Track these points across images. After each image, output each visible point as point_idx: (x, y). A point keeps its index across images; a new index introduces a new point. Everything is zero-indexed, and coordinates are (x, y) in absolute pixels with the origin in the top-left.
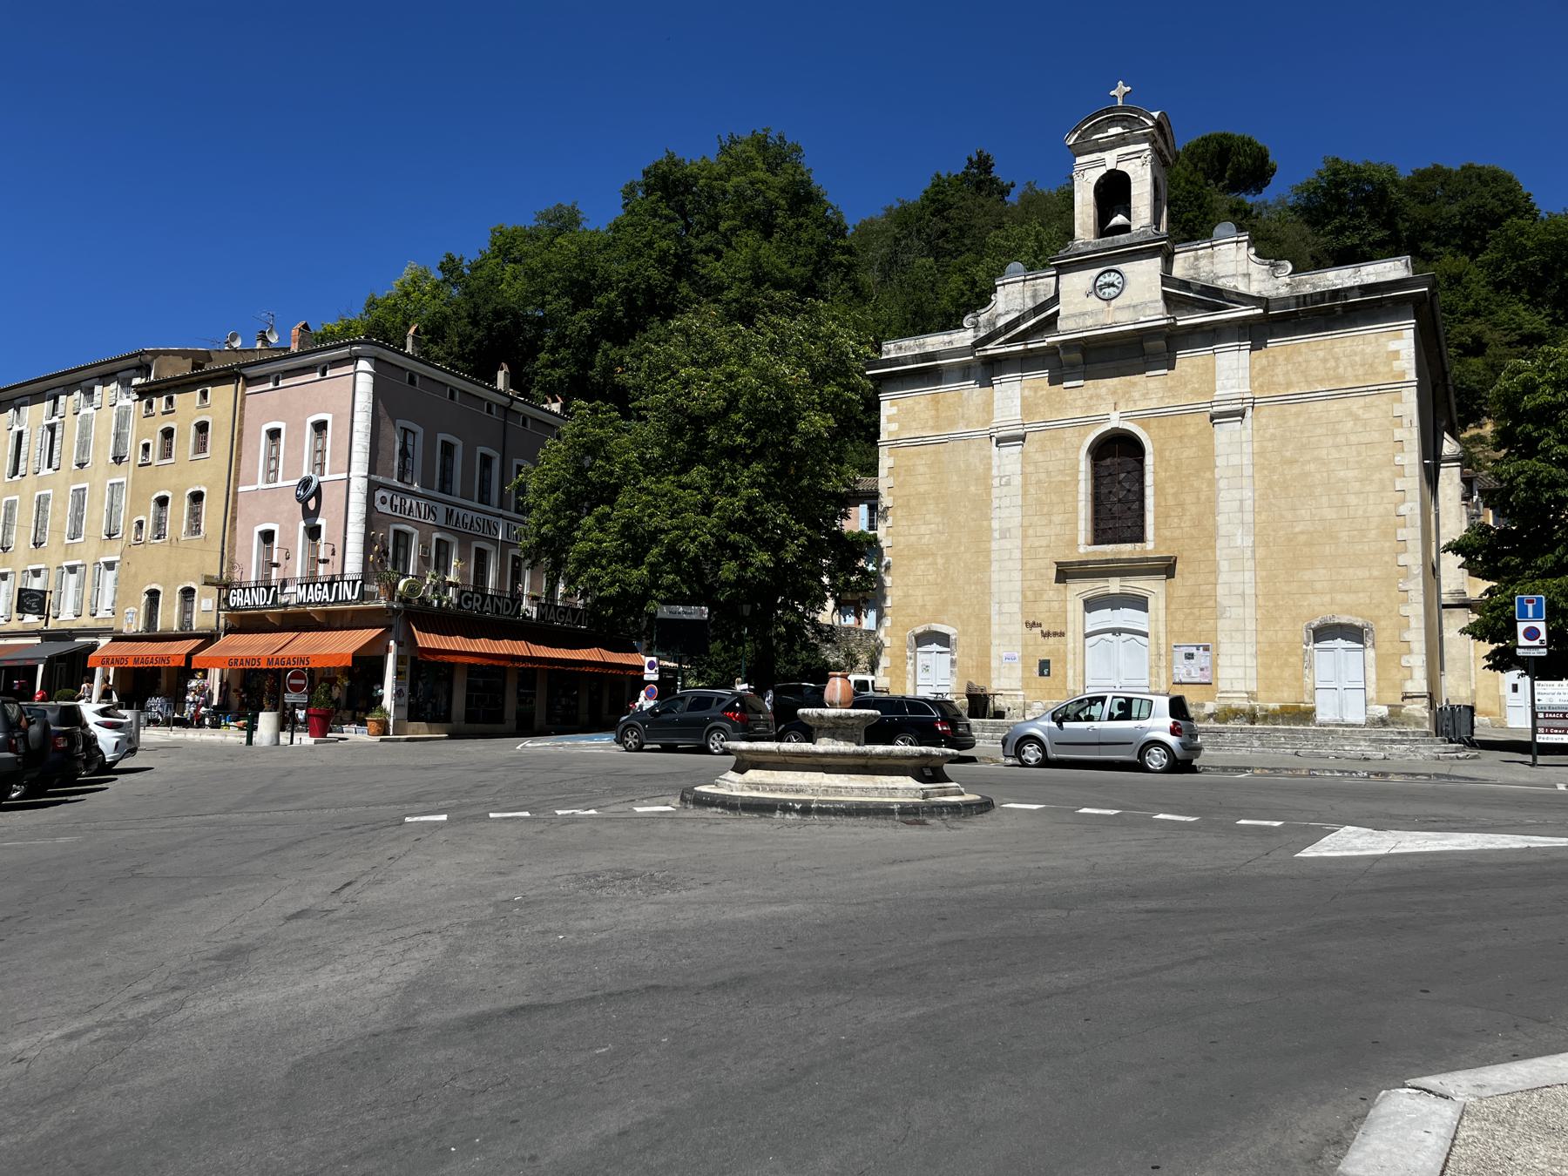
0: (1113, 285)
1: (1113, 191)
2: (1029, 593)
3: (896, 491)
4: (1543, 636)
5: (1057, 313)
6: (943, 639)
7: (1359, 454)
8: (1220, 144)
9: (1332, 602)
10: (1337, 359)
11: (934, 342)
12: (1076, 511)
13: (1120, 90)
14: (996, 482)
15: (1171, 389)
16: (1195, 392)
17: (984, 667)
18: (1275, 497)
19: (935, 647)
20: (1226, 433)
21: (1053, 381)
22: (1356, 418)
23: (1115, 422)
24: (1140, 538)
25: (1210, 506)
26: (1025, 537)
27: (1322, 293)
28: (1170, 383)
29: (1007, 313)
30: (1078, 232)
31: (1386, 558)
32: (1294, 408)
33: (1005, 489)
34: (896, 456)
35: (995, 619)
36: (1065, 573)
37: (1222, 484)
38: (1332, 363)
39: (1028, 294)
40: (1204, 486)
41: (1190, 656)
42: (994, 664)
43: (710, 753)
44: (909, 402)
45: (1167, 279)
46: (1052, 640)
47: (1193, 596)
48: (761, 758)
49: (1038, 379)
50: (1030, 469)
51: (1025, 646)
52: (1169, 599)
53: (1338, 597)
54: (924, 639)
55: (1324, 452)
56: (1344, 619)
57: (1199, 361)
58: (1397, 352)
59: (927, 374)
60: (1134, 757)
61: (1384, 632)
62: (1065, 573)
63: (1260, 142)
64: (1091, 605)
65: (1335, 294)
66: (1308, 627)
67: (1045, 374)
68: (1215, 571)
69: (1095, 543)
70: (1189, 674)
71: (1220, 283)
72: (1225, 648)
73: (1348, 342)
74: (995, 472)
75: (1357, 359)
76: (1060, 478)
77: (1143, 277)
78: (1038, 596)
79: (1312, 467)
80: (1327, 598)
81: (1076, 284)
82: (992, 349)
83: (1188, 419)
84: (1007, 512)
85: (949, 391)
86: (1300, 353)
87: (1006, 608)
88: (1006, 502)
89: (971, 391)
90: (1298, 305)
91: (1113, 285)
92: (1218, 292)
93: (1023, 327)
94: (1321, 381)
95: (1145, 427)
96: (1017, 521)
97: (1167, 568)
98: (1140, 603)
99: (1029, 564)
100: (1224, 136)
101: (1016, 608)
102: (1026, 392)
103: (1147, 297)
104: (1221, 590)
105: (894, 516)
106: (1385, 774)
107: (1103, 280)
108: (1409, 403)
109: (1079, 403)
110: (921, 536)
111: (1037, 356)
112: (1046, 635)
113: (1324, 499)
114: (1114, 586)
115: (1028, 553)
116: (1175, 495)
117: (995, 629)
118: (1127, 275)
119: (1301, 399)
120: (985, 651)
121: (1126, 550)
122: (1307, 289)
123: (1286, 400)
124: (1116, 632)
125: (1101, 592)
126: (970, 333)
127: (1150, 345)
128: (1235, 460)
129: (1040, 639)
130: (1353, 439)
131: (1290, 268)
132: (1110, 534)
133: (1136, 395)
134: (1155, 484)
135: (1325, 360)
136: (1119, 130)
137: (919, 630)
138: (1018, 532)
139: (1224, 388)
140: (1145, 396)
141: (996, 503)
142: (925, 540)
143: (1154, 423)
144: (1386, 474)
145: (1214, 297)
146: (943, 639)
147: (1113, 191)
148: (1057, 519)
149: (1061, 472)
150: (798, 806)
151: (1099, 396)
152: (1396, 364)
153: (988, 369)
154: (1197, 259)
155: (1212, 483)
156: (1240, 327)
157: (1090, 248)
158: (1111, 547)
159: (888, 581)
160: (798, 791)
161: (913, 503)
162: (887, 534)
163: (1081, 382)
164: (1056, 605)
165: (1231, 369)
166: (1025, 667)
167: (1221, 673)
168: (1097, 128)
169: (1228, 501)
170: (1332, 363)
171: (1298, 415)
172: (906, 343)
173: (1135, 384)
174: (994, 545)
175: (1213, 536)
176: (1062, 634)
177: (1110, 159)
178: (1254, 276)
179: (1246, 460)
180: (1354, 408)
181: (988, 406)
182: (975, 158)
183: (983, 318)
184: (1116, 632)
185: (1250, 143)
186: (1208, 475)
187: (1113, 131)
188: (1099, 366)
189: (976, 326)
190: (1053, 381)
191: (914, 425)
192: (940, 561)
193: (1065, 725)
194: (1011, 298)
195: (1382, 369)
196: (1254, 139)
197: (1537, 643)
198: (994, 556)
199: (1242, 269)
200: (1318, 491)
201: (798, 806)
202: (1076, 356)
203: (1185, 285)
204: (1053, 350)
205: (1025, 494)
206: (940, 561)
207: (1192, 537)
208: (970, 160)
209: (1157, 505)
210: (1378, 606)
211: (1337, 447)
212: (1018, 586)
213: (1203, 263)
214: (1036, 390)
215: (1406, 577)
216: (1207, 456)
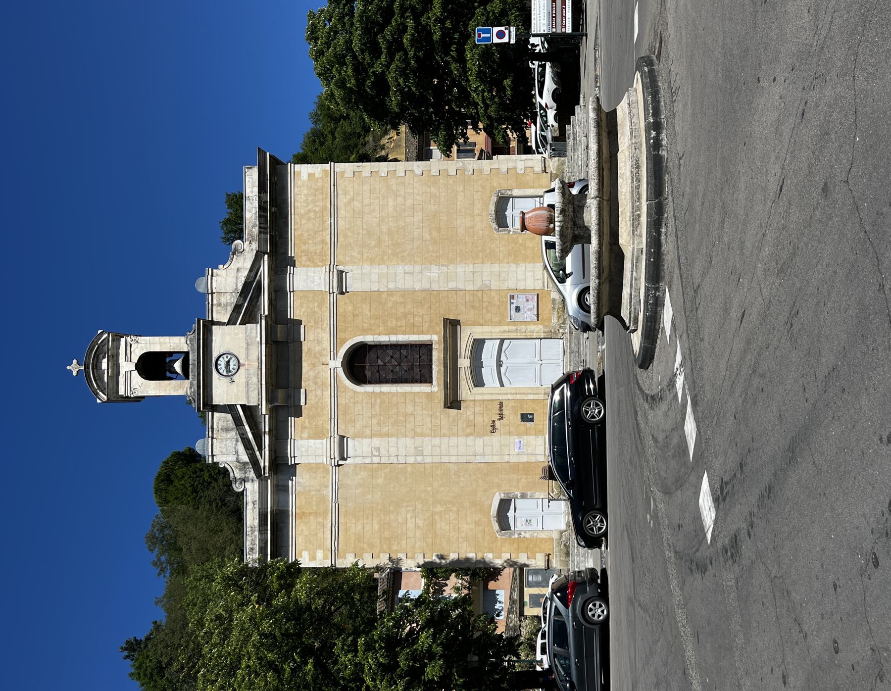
0: (228, 362)
1: (154, 366)
2: (468, 431)
3: (376, 551)
4: (503, 28)
5: (242, 406)
6: (505, 505)
7: (378, 198)
8: (163, 481)
9: (480, 215)
10: (309, 211)
11: (251, 518)
12: (404, 394)
13: (74, 368)
14: (376, 460)
15: (316, 323)
16: (320, 306)
17: (526, 468)
18: (404, 252)
19: (511, 514)
20: (353, 284)
21: (298, 413)
22: (353, 199)
23: (337, 363)
24: (427, 347)
25: (408, 294)
26: (422, 435)
27: (260, 216)
28: (312, 323)
29: (237, 452)
30: (181, 392)
31: (451, 182)
32: (341, 239)
33: (383, 452)
34: (345, 552)
35: (488, 459)
36: (453, 402)
37: (391, 286)
38: (312, 215)
39: (224, 434)
40: (393, 299)
41: (518, 309)
42: (524, 459)
43: (607, 618)
44: (300, 540)
45: (232, 322)
46: (505, 412)
47: (473, 307)
48: (606, 230)
49: (294, 423)
50: (368, 431)
51: (510, 433)
52: (475, 323)
53: (477, 212)
54: (504, 523)
55: (374, 219)
56: (492, 208)
57: (297, 303)
58: (309, 175)
59: (278, 524)
60: (597, 629)
61: (502, 185)
62: (453, 402)
63: (167, 456)
64: (478, 382)
65: (262, 208)
66: (497, 231)
67: (292, 420)
68: (456, 291)
69: (431, 382)
70: (531, 310)
71: (240, 287)
72: (512, 285)
73: (298, 204)
74: (367, 461)
75: (310, 199)
76: (377, 407)
77: (224, 339)
78: (470, 424)
79: (384, 228)
80: (478, 219)
81: (223, 391)
82: (265, 462)
83: (340, 310)
84: (400, 449)
85: (295, 503)
86: (302, 235)
87: (479, 450)
88: (393, 451)
89: (299, 484)
90: (266, 233)
91: (228, 362)
92: (247, 285)
93: (250, 436)
94: (324, 222)
95: (344, 341)
96: (409, 441)
97: (452, 326)
98: (478, 345)
99: (445, 431)
100: (157, 479)
101: (480, 442)
102: (305, 435)
103: (242, 336)
104: (470, 287)
105: (397, 552)
106: (596, 77)
107: (223, 370)
108: (346, 169)
109: (319, 393)
110: (417, 526)
111: (277, 428)
112: (501, 417)
113: (408, 220)
114: (464, 363)
115: (436, 432)
116: (398, 319)
117: (496, 459)
118: (222, 352)
119: (334, 234)
120: (515, 468)
121: (437, 356)
122: (256, 231)
123: (334, 245)
124: (499, 364)
125: (469, 374)
126: (248, 485)
127: (280, 336)
128: (374, 277)
129: (505, 421)
130: (366, 201)
131: (239, 241)
132: (425, 371)
133: (318, 348)
134: (388, 334)
135: (309, 219)
136: (105, 361)
137: (496, 527)
138: (418, 441)
139: (320, 284)
140: (319, 342)
141: (393, 460)
142: (420, 522)
143: (341, 335)
144: (393, 182)
145: (250, 289)
146: (505, 505)
147: (154, 366)
148: (410, 409)
149: (373, 406)
150: (653, 134)
151: (316, 377)
152: (317, 175)
153: (281, 468)
154: (219, 305)
155: (390, 293)
156: (276, 273)
157: (195, 382)
158: (434, 367)
159: (453, 556)
160: (638, 167)
161: (387, 534)
162: (413, 558)
163: (302, 391)
164: (478, 409)
165: (306, 280)
166: (527, 433)
167: (530, 285)
168: (99, 378)
169: (408, 283)
170: (312, 215)
171: (346, 236)
172: (248, 544)
173: (309, 350)
174: (428, 460)
175: (429, 292)
176: (501, 404)
177: (127, 366)
178: (240, 265)
179: (376, 270)
180: (345, 200)
181: (314, 468)
182: (126, 653)
183: (238, 474)
184: (499, 364)
185: (166, 462)
186: (384, 296)
187: (104, 365)
188: (291, 377)
189: (244, 480)
190: (298, 413)
191: (320, 535)
192: (439, 508)
193: (568, 271)
194: (224, 448)
195: (320, 184)
196: (165, 459)
197: (507, 32)
198: (437, 460)
199: (233, 273)
200: (402, 223)
201: (653, 134)
202: (281, 393)
203: (237, 308)
204: (274, 411)
205: (388, 435)
206: (439, 508)
207: (430, 308)
208: (127, 657)
209: (404, 333)
210: (483, 187)
211: (371, 212)
212: (462, 440)
213: (223, 300)
214: (304, 428)
215: (464, 170)
216: (368, 296)
